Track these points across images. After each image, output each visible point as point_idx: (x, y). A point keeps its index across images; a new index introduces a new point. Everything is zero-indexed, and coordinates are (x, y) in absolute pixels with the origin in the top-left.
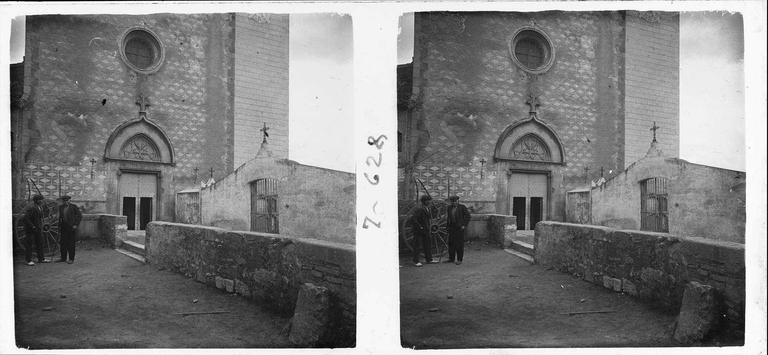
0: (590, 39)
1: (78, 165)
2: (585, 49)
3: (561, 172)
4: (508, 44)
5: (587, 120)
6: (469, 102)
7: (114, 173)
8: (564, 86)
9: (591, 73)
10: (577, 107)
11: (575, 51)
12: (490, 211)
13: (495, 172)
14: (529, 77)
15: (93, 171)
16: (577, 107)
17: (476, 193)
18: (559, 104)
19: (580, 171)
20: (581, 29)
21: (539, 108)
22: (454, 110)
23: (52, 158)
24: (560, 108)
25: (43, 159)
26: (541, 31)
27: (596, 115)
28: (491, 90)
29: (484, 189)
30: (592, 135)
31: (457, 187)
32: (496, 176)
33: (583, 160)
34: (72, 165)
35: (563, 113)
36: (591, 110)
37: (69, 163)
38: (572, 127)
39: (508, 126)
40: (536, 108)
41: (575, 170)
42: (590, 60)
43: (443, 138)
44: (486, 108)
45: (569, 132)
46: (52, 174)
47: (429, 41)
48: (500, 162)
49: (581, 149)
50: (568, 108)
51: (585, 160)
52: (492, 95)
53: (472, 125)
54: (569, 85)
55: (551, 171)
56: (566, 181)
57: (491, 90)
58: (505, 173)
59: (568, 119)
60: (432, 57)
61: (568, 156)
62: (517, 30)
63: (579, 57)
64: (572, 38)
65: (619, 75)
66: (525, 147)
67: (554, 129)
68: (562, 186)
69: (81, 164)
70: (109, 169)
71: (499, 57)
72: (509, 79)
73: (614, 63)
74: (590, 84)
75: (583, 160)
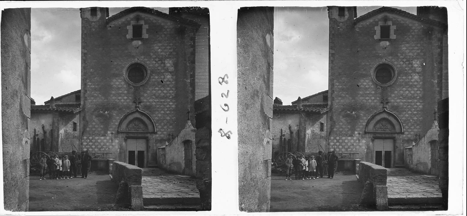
0: (171, 60)
1: (105, 136)
2: (415, 67)
3: (154, 137)
4: (123, 73)
5: (170, 107)
6: (105, 105)
7: (123, 139)
8: (403, 90)
9: (419, 80)
10: (410, 101)
11: (161, 69)
12: (356, 158)
13: (119, 138)
14: (383, 89)
15: (112, 138)
16: (410, 101)
17: (356, 149)
18: (400, 101)
19: (413, 136)
20: (413, 57)
21: (388, 104)
22: (346, 110)
23: (341, 134)
24: (152, 103)
25: (336, 134)
26: (389, 63)
27: (175, 104)
28: (363, 98)
29: (360, 147)
30: (420, 116)
31: (348, 146)
32: (366, 141)
33: (414, 130)
34: (103, 136)
35: (155, 105)
36: (419, 101)
37: (101, 135)
38: (160, 112)
39: (124, 115)
40: (386, 104)
41: (409, 136)
42: (418, 73)
43: (341, 124)
44: (361, 107)
45: (405, 115)
46: (93, 141)
47: (87, 79)
48: (120, 134)
49: (413, 124)
50: (405, 102)
51: (416, 130)
52: (363, 101)
53: (354, 116)
54: (158, 89)
55: (148, 137)
56: (157, 142)
57: (363, 98)
58: (371, 139)
59: (405, 108)
60: (88, 86)
61: (405, 128)
62: (128, 65)
63: (411, 72)
64: (160, 62)
65: (438, 78)
66: (381, 125)
67: (397, 114)
68: (154, 145)
69: (354, 135)
70: (367, 137)
71: (119, 80)
72: (372, 91)
73: (435, 72)
74: (171, 86)
75: (414, 130)
